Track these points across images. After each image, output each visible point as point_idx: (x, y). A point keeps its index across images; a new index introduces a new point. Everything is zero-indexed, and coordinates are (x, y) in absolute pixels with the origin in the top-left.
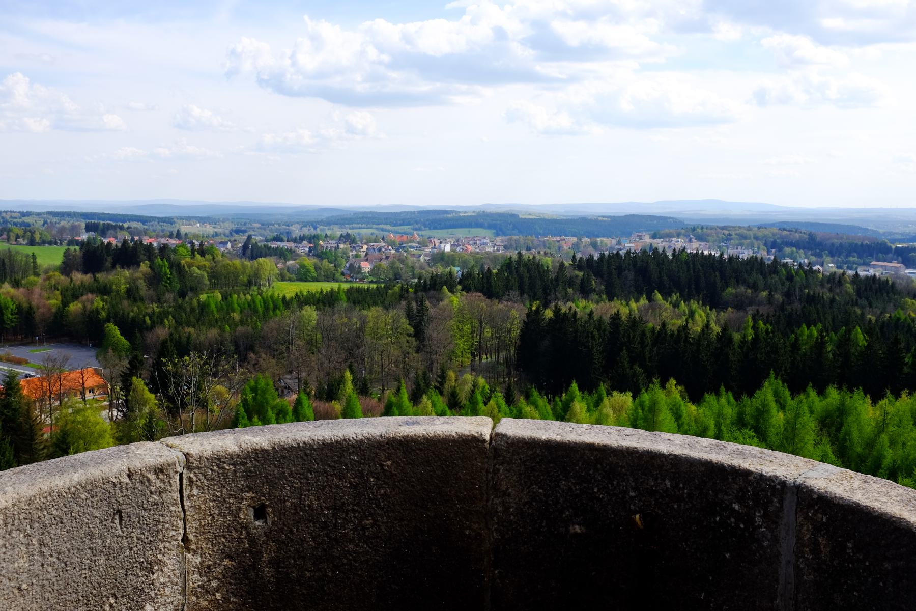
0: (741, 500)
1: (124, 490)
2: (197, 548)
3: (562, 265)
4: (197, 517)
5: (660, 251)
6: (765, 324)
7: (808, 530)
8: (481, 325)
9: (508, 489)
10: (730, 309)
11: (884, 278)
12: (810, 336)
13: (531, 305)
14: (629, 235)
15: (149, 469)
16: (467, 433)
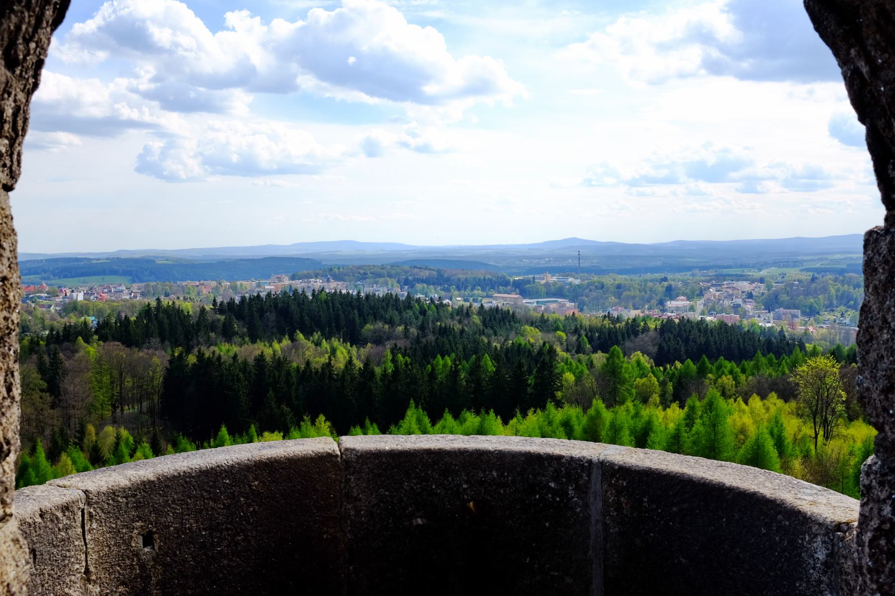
0: (555, 479)
1: (38, 529)
2: (97, 579)
3: (203, 310)
4: (96, 549)
5: (300, 291)
6: (404, 357)
7: (612, 494)
8: (121, 375)
9: (358, 494)
10: (369, 344)
11: (505, 309)
12: (445, 365)
13: (173, 352)
14: (268, 277)
15: (57, 508)
16: (321, 451)
